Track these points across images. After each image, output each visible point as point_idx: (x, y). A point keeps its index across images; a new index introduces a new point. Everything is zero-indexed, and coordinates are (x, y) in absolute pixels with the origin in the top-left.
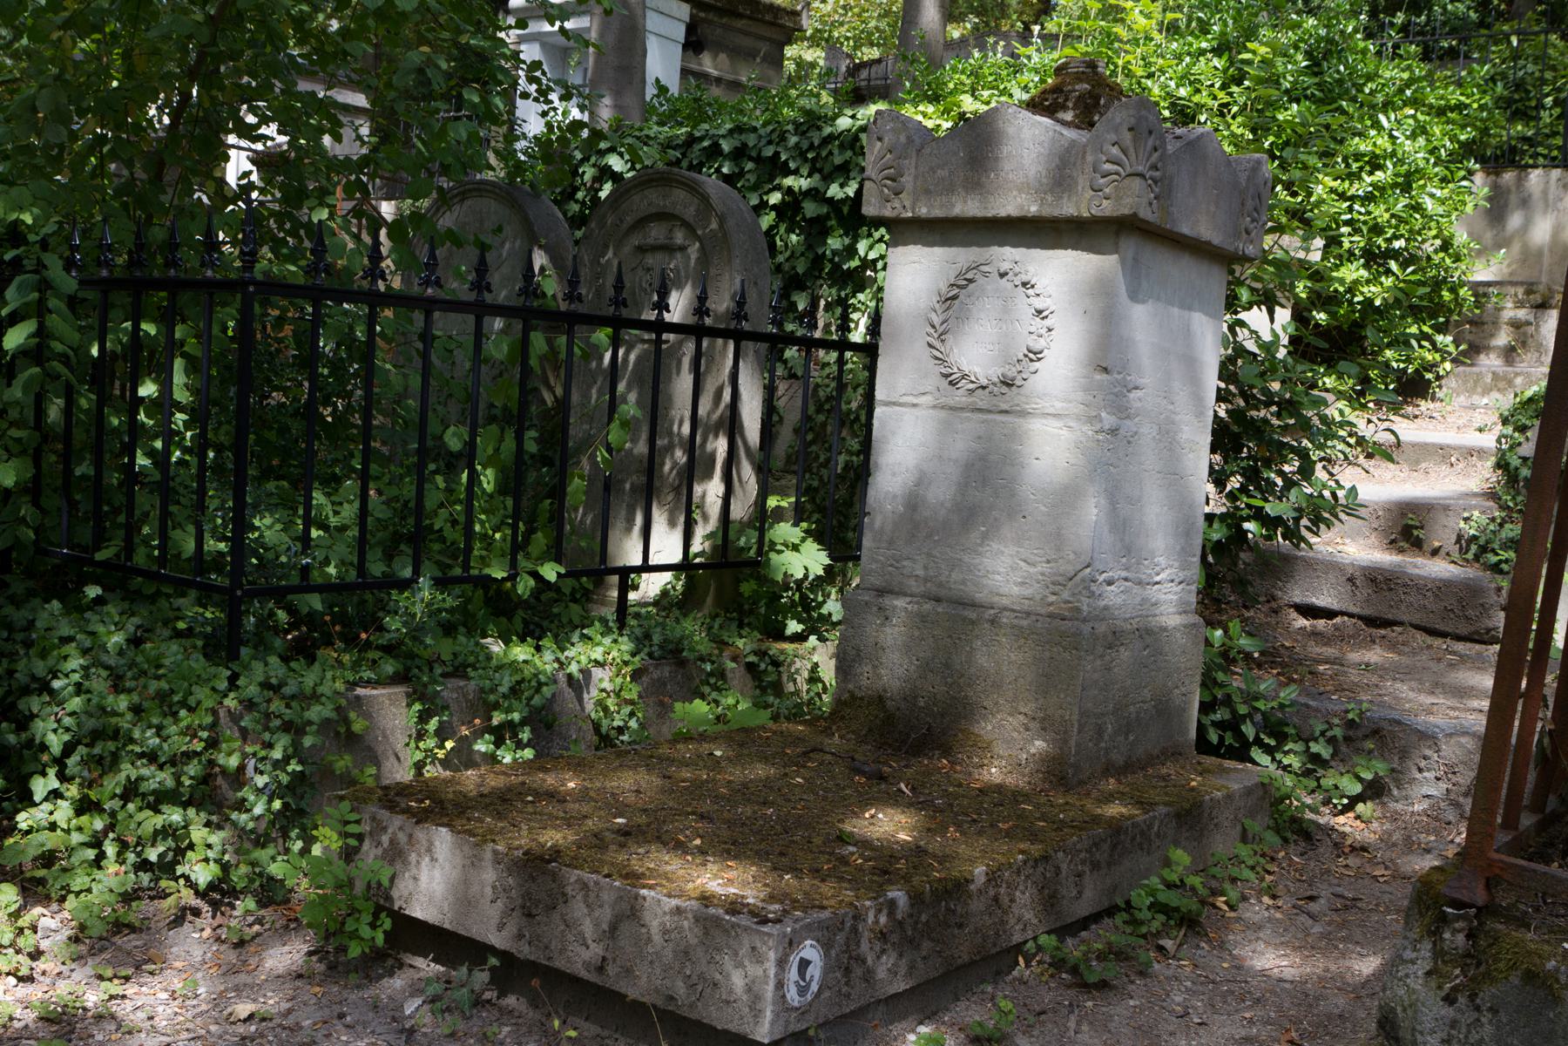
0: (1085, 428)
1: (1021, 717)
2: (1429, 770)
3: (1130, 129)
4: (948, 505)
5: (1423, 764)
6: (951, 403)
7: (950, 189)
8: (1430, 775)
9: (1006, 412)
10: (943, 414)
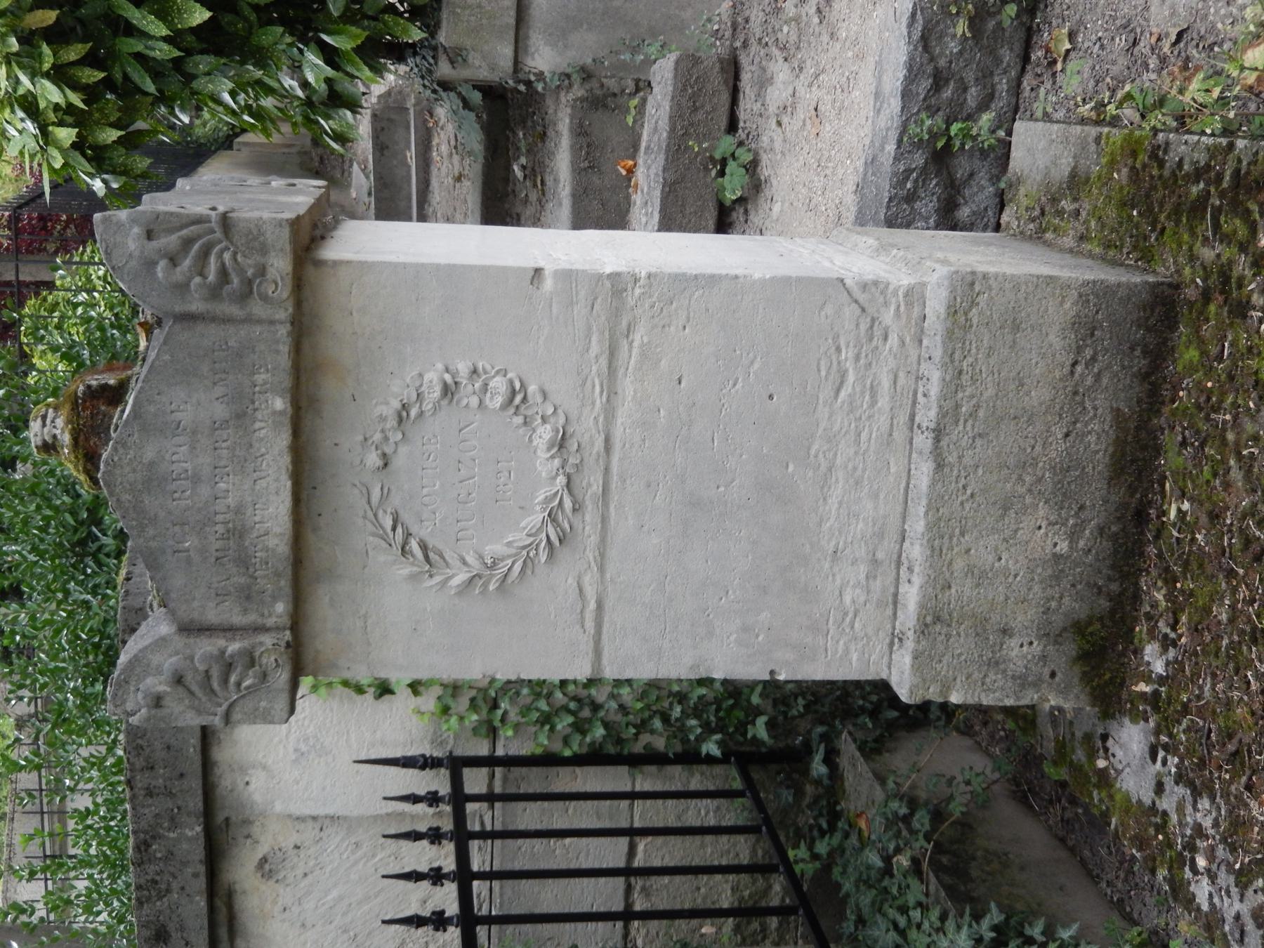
9: (607, 440)
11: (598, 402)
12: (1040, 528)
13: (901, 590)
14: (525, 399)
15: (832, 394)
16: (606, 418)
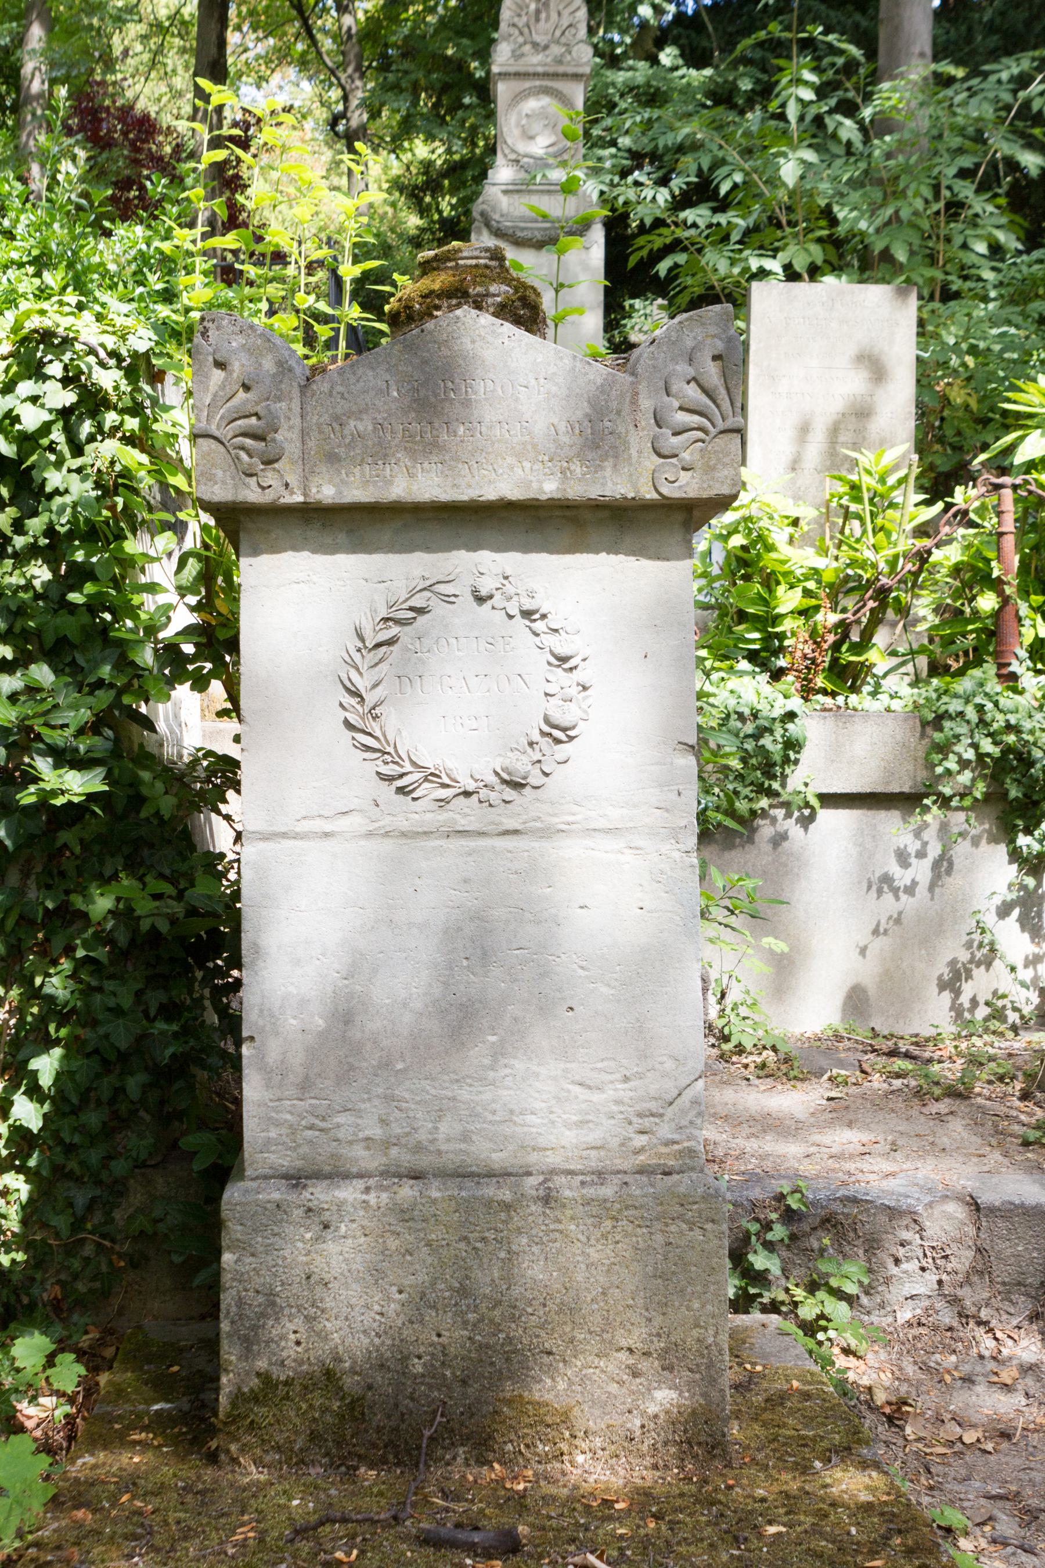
0: (666, 847)
1: (623, 1356)
2: (908, 1259)
3: (716, 358)
4: (418, 1005)
5: (901, 1252)
6: (405, 825)
7: (380, 454)
8: (912, 1266)
9: (516, 832)
10: (388, 846)
11: (557, 820)
12: (439, 1335)
13: (355, 1182)
14: (558, 741)
15: (577, 1078)
16: (539, 829)
